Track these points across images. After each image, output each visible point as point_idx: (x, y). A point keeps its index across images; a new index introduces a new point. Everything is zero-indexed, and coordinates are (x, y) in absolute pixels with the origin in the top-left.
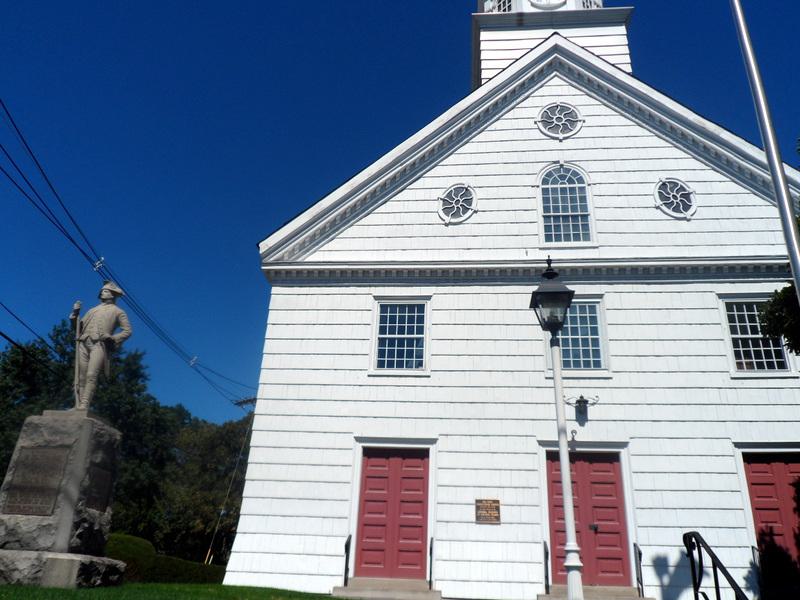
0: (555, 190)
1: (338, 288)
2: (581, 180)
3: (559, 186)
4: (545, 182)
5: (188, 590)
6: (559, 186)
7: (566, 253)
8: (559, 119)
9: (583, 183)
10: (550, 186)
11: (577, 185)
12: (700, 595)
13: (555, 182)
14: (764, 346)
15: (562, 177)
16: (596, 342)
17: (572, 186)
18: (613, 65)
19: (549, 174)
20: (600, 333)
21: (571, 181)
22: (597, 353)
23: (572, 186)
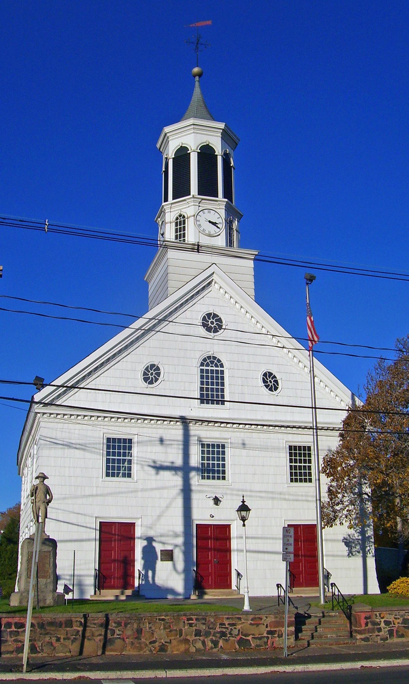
0: (207, 371)
1: (201, 523)
2: (222, 366)
3: (209, 368)
4: (202, 364)
5: (89, 579)
6: (209, 368)
7: (244, 537)
8: (212, 323)
9: (223, 367)
10: (205, 368)
11: (219, 369)
12: (280, 599)
13: (208, 365)
14: (297, 459)
15: (212, 362)
16: (202, 383)
17: (217, 369)
18: (240, 288)
19: (205, 360)
20: (211, 405)
21: (216, 366)
22: (202, 377)
23: (217, 369)
